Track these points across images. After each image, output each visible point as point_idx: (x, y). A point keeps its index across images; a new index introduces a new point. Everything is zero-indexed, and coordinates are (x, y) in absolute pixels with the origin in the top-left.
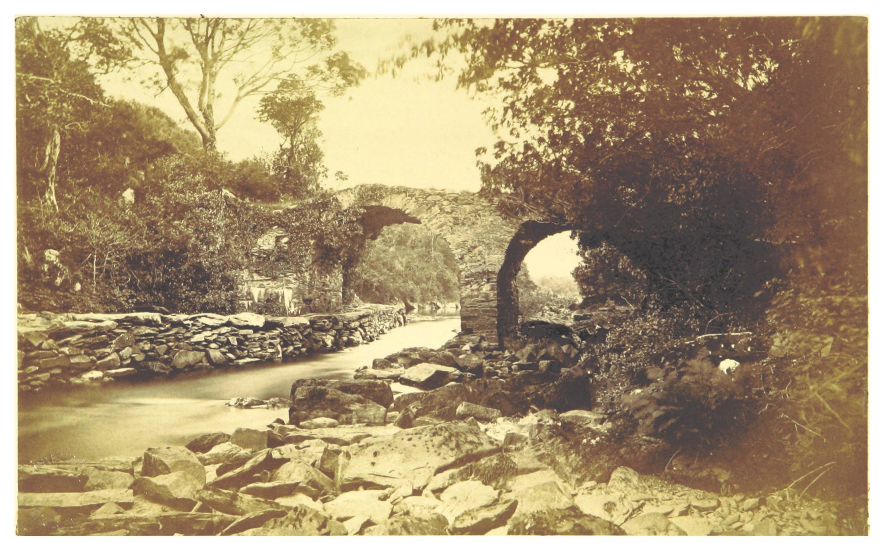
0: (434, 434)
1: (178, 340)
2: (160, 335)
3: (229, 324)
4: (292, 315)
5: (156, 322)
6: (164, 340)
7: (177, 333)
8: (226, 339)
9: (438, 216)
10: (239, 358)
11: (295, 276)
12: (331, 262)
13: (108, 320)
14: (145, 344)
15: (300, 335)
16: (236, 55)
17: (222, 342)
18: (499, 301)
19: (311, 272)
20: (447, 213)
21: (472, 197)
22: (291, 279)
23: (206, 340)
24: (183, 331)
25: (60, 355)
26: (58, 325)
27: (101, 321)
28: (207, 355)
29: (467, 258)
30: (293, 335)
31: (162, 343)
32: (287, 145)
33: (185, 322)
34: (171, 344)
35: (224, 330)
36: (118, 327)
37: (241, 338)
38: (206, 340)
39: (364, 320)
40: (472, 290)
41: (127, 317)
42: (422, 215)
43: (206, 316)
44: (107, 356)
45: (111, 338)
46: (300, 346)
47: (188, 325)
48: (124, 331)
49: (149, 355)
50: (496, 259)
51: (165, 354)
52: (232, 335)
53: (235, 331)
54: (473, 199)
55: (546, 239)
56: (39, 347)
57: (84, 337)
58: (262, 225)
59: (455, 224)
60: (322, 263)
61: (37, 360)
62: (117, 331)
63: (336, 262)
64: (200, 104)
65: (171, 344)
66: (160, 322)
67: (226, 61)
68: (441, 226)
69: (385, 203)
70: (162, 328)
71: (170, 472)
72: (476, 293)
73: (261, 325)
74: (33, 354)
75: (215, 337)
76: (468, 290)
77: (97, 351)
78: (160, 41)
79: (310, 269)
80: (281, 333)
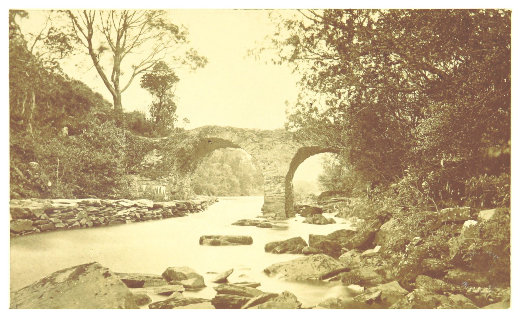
0: (315, 260)
1: (110, 214)
2: (102, 211)
3: (135, 206)
4: (166, 201)
5: (98, 204)
7: (109, 211)
9: (251, 144)
11: (167, 178)
13: (73, 203)
14: (93, 216)
16: (132, 49)
17: (132, 216)
18: (286, 193)
19: (175, 176)
20: (256, 142)
21: (271, 133)
23: (124, 215)
24: (113, 209)
26: (49, 206)
27: (69, 203)
29: (267, 168)
31: (102, 216)
32: (157, 101)
34: (106, 217)
35: (133, 209)
36: (78, 207)
37: (143, 214)
38: (124, 215)
40: (271, 187)
42: (242, 143)
43: (123, 201)
44: (73, 223)
45: (75, 213)
47: (115, 206)
48: (82, 209)
49: (95, 223)
51: (103, 222)
52: (137, 212)
53: (139, 209)
54: (271, 134)
55: (309, 158)
57: (62, 212)
59: (260, 149)
60: (181, 171)
61: (39, 225)
62: (78, 209)
63: (188, 171)
64: (113, 77)
65: (106, 217)
66: (101, 204)
67: (127, 52)
68: (253, 150)
70: (101, 208)
71: (187, 279)
73: (152, 206)
76: (269, 187)
77: (68, 220)
78: (89, 40)
79: (175, 174)
80: (162, 211)
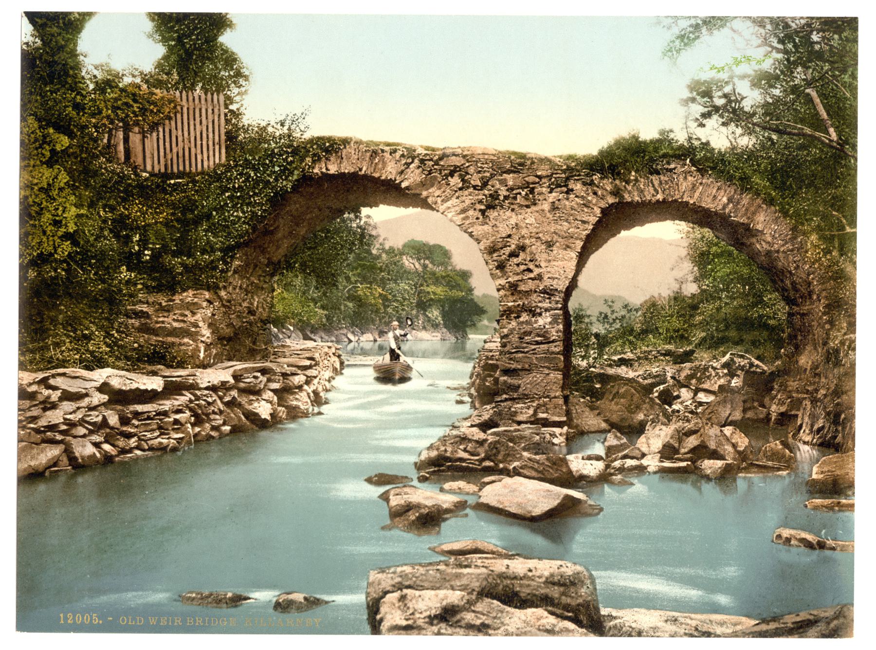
8: (100, 418)
10: (123, 451)
15: (219, 402)
17: (94, 424)
23: (67, 422)
28: (68, 451)
30: (209, 404)
46: (221, 422)
75: (79, 415)
80: (191, 401)
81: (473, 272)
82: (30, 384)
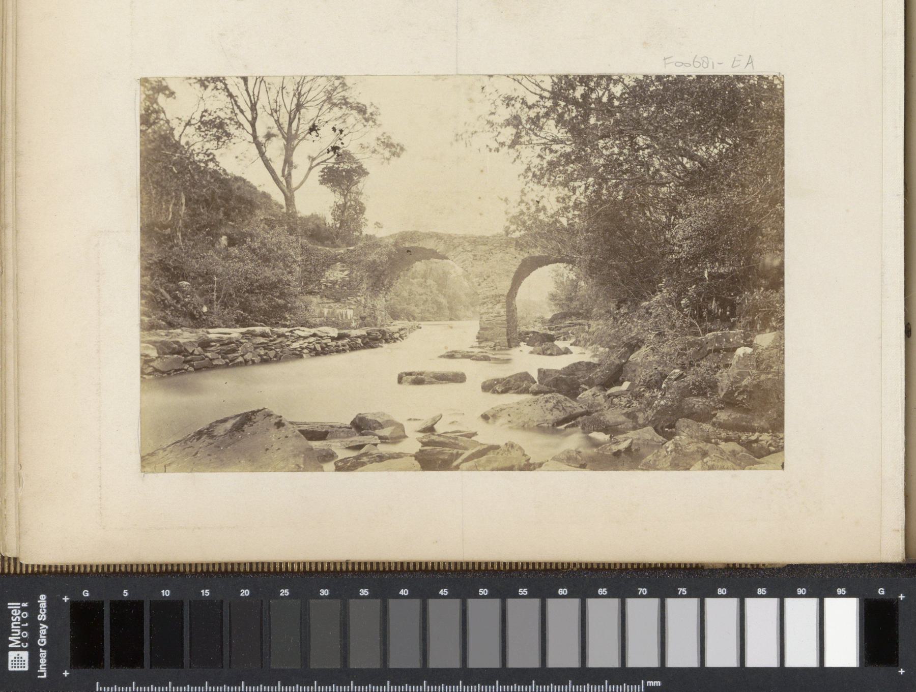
1: (282, 347)
2: (271, 343)
3: (314, 335)
4: (353, 328)
6: (273, 348)
8: (313, 347)
11: (355, 299)
12: (378, 289)
18: (507, 316)
19: (365, 296)
22: (352, 302)
23: (300, 347)
25: (206, 359)
27: (230, 334)
29: (483, 285)
31: (272, 349)
32: (341, 201)
33: (287, 334)
35: (312, 339)
37: (324, 346)
38: (300, 347)
39: (402, 332)
41: (248, 330)
43: (299, 330)
45: (238, 346)
48: (247, 341)
50: (505, 285)
52: (317, 343)
53: (319, 340)
56: (192, 354)
57: (221, 345)
58: (330, 262)
63: (381, 289)
65: (278, 350)
69: (421, 244)
70: (271, 339)
71: (383, 428)
72: (491, 310)
73: (336, 336)
74: (189, 358)
75: (306, 345)
77: (229, 356)
78: (253, 124)
81: (467, 380)
82: (287, 332)
